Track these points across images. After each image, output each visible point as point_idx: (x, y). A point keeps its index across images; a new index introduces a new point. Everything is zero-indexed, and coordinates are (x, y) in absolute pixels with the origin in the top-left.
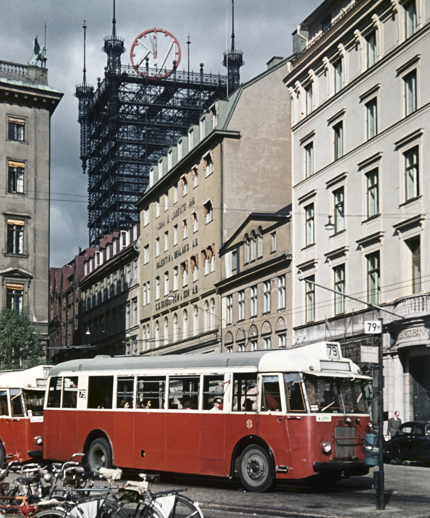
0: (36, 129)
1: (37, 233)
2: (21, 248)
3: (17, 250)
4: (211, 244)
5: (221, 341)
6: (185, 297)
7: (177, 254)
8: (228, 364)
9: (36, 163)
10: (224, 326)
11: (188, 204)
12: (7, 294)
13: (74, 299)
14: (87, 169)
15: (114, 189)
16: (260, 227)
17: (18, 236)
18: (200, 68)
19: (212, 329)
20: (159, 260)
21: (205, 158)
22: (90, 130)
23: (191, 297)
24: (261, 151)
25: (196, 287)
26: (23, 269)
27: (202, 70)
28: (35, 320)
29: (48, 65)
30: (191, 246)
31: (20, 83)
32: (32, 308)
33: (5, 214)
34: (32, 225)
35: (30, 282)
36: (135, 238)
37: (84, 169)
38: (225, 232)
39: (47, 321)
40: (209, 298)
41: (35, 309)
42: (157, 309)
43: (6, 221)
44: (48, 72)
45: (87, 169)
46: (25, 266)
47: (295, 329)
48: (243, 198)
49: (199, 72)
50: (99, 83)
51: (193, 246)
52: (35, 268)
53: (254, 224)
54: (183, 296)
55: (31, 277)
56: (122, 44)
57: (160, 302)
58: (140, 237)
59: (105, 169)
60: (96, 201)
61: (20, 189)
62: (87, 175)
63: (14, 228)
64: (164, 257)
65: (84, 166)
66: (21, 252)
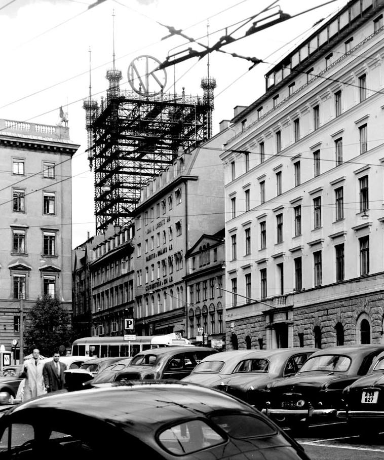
0: (61, 169)
1: (64, 240)
2: (53, 252)
3: (51, 253)
4: (180, 251)
5: (187, 315)
6: (165, 283)
7: (160, 253)
8: (141, 341)
9: (62, 193)
10: (188, 305)
11: (166, 220)
12: (44, 283)
13: (85, 277)
14: (93, 167)
15: (115, 156)
16: (208, 244)
17: (51, 243)
18: (182, 90)
19: (181, 306)
20: (148, 255)
21: (176, 192)
22: (95, 136)
23: (169, 284)
24: (212, 189)
25: (172, 277)
26: (54, 265)
27: (183, 92)
28: (63, 300)
29: (69, 125)
30: (168, 249)
31: (51, 140)
32: (61, 292)
33: (42, 229)
34: (60, 236)
35: (59, 274)
36: (131, 237)
37: (91, 168)
38: (189, 243)
39: (71, 301)
40: (179, 286)
41: (62, 292)
42: (146, 290)
43: (43, 233)
44: (70, 129)
45: (93, 167)
46: (56, 263)
47: (227, 310)
48: (200, 220)
49: (182, 94)
50: (102, 101)
51: (170, 249)
52: (62, 265)
53: (206, 241)
54: (163, 282)
55: (60, 271)
56: (121, 73)
57: (149, 285)
58: (135, 237)
59: (108, 154)
60: (101, 195)
61: (51, 211)
62: (93, 173)
63: (49, 238)
64: (151, 254)
65: (91, 166)
66: (53, 254)
